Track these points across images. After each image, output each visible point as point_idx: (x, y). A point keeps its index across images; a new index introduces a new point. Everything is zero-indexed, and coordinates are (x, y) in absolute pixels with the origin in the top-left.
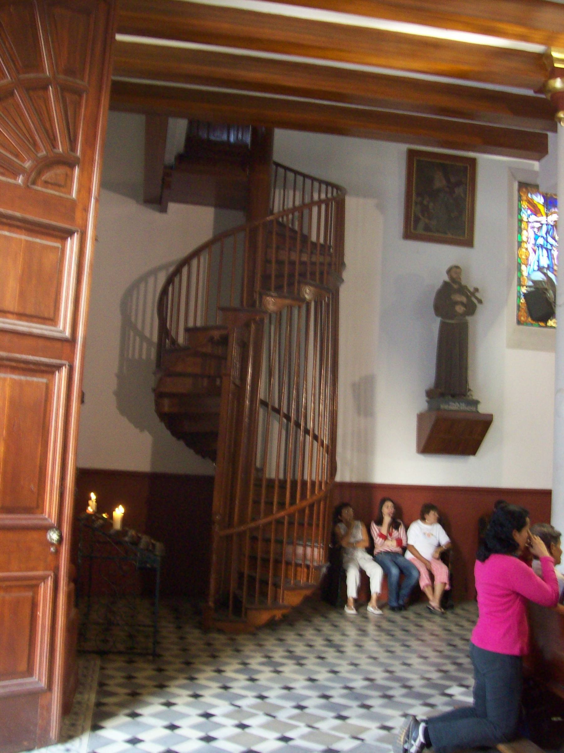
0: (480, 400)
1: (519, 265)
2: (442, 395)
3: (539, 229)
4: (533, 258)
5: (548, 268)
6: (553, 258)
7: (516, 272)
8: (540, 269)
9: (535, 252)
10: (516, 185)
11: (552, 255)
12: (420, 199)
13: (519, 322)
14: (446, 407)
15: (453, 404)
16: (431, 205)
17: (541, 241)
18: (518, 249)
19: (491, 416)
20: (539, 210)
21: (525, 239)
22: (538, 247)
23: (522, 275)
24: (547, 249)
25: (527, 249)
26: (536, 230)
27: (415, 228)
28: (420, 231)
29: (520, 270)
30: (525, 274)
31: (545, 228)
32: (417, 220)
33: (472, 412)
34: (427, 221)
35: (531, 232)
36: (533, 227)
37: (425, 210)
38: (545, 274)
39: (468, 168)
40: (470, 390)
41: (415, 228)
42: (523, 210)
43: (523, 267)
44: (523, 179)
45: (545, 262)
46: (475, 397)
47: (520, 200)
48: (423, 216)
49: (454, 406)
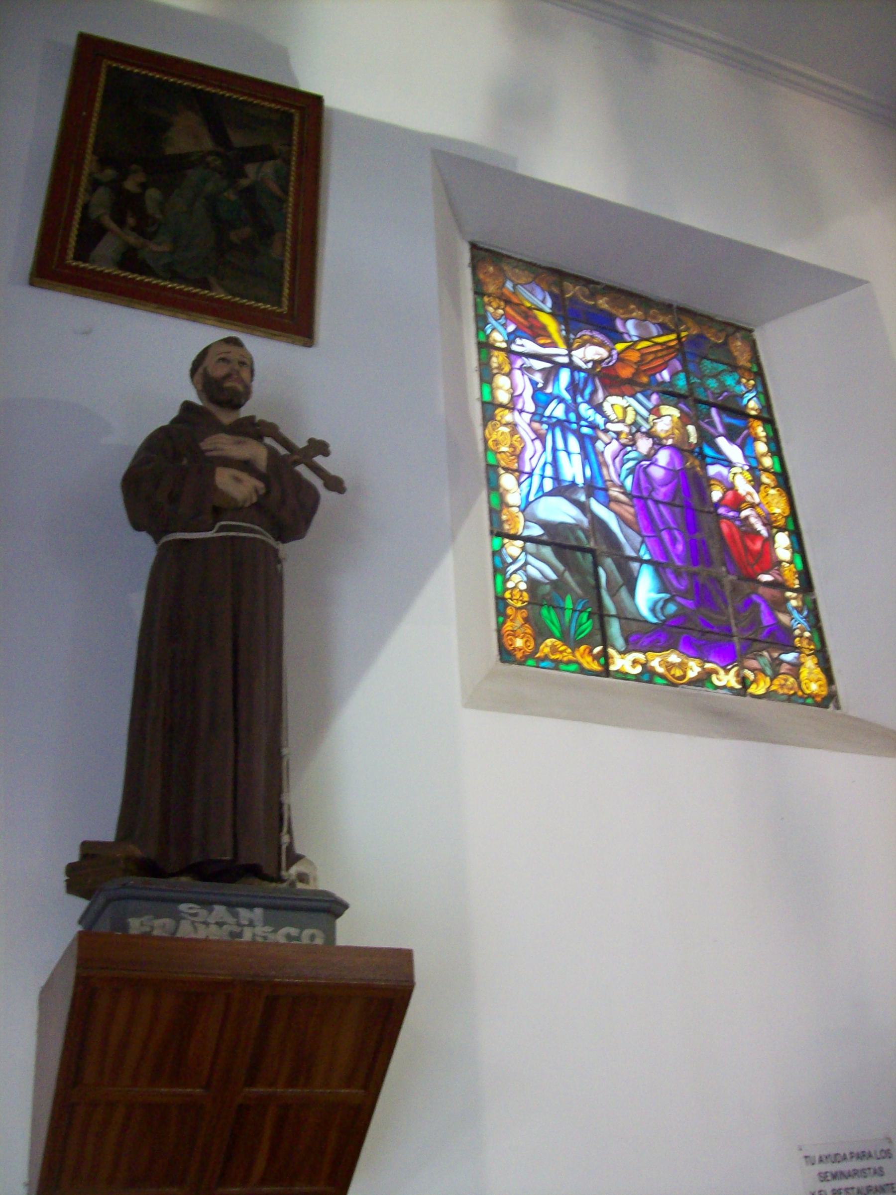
0: (341, 894)
1: (492, 472)
2: (150, 869)
3: (551, 374)
4: (535, 456)
5: (591, 488)
6: (602, 464)
7: (484, 494)
8: (563, 489)
9: (541, 438)
10: (466, 256)
11: (599, 454)
12: (110, 173)
13: (506, 654)
14: (160, 926)
15: (203, 912)
16: (153, 194)
17: (558, 411)
18: (485, 426)
19: (402, 959)
20: (544, 328)
21: (503, 397)
22: (552, 427)
23: (504, 504)
24: (581, 438)
25: (514, 426)
26: (538, 377)
27: (83, 253)
28: (104, 259)
29: (494, 486)
30: (514, 498)
31: (565, 375)
32: (92, 234)
33: (311, 949)
34: (132, 239)
35: (522, 382)
36: (530, 369)
37: (125, 205)
38: (583, 508)
39: (297, 119)
40: (294, 858)
41: (83, 253)
42: (491, 320)
43: (507, 481)
44: (484, 241)
45: (573, 469)
46: (327, 880)
47: (479, 292)
48: (121, 223)
49: (208, 924)
